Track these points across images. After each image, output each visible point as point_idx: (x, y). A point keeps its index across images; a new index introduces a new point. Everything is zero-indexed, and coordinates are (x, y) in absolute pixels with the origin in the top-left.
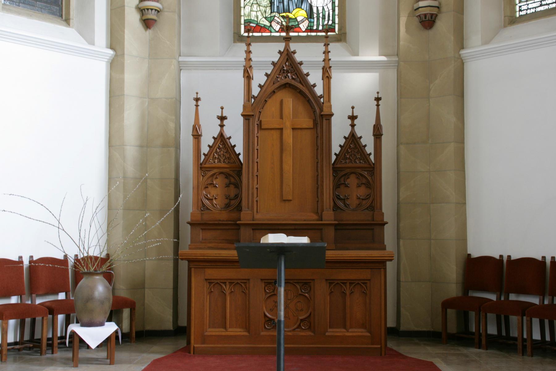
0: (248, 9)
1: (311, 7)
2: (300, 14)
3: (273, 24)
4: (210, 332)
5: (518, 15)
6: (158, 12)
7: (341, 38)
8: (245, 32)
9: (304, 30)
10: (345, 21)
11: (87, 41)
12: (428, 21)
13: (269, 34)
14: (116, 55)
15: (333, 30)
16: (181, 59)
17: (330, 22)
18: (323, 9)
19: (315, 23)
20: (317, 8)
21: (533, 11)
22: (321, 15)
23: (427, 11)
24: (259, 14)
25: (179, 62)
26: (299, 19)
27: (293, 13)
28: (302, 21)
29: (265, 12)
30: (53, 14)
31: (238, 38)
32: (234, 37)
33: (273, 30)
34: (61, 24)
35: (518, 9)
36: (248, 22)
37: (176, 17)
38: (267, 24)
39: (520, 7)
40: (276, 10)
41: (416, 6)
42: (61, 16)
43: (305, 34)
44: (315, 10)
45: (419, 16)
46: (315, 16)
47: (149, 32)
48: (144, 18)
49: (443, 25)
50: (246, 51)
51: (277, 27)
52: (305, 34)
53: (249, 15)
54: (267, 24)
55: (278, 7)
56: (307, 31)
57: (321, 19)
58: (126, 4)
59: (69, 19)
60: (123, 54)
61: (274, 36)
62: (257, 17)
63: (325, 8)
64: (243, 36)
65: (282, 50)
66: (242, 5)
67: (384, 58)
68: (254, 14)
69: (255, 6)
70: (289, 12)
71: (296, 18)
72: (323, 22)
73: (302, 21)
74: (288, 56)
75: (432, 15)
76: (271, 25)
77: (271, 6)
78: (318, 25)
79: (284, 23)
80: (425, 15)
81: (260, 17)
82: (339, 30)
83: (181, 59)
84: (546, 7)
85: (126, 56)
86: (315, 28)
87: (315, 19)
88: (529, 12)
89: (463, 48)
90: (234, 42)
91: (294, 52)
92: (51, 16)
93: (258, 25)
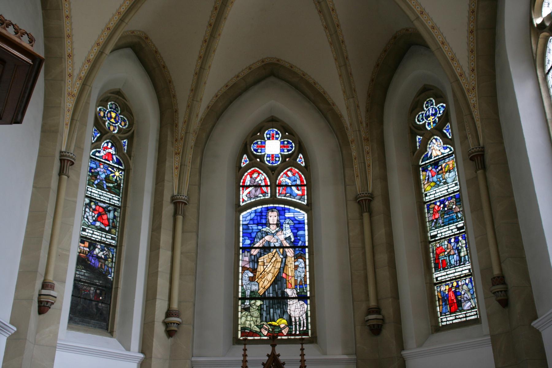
0: (243, 319)
1: (290, 317)
2: (282, 322)
3: (263, 330)
4: (470, 316)
5: (440, 325)
6: (179, 324)
7: (313, 340)
8: (241, 336)
9: (285, 334)
10: (315, 327)
11: (124, 348)
12: (376, 330)
13: (259, 338)
14: (145, 358)
15: (307, 335)
16: (193, 359)
17: (305, 328)
18: (299, 318)
19: (294, 329)
20: (295, 317)
21: (451, 322)
22: (298, 323)
23: (375, 322)
24: (252, 323)
25: (192, 361)
26: (282, 326)
27: (277, 321)
28: (284, 328)
29: (256, 321)
30: (101, 328)
31: (237, 341)
32: (233, 340)
33: (262, 335)
34: (106, 336)
35: (440, 320)
36: (243, 329)
37: (191, 328)
38: (258, 330)
39: (441, 319)
40: (264, 320)
41: (366, 318)
42: (107, 329)
43: (286, 337)
44: (293, 320)
45: (369, 326)
46: (294, 323)
47: (171, 339)
48: (168, 329)
49: (388, 332)
50: (243, 355)
51: (266, 333)
52: (286, 337)
53: (245, 323)
54: (258, 330)
55: (266, 317)
56: (287, 335)
57: (298, 326)
58: (156, 320)
59: (113, 332)
60: (151, 358)
61: (263, 339)
62: (250, 325)
63: (301, 318)
64: (239, 339)
65: (270, 354)
66: (240, 316)
67: (346, 357)
68: (248, 323)
69: (249, 317)
70: (274, 321)
71: (279, 326)
72: (300, 328)
73: (284, 328)
74: (273, 357)
75: (378, 325)
76: (261, 331)
77: (261, 317)
78: (296, 330)
79: (270, 329)
80: (374, 325)
81: (253, 325)
82: (311, 334)
83: (193, 359)
84: (459, 320)
85: (153, 359)
86: (294, 333)
87: (294, 326)
88: (448, 323)
89: (403, 349)
90: (233, 345)
91: (279, 355)
92: (100, 330)
93: (251, 331)
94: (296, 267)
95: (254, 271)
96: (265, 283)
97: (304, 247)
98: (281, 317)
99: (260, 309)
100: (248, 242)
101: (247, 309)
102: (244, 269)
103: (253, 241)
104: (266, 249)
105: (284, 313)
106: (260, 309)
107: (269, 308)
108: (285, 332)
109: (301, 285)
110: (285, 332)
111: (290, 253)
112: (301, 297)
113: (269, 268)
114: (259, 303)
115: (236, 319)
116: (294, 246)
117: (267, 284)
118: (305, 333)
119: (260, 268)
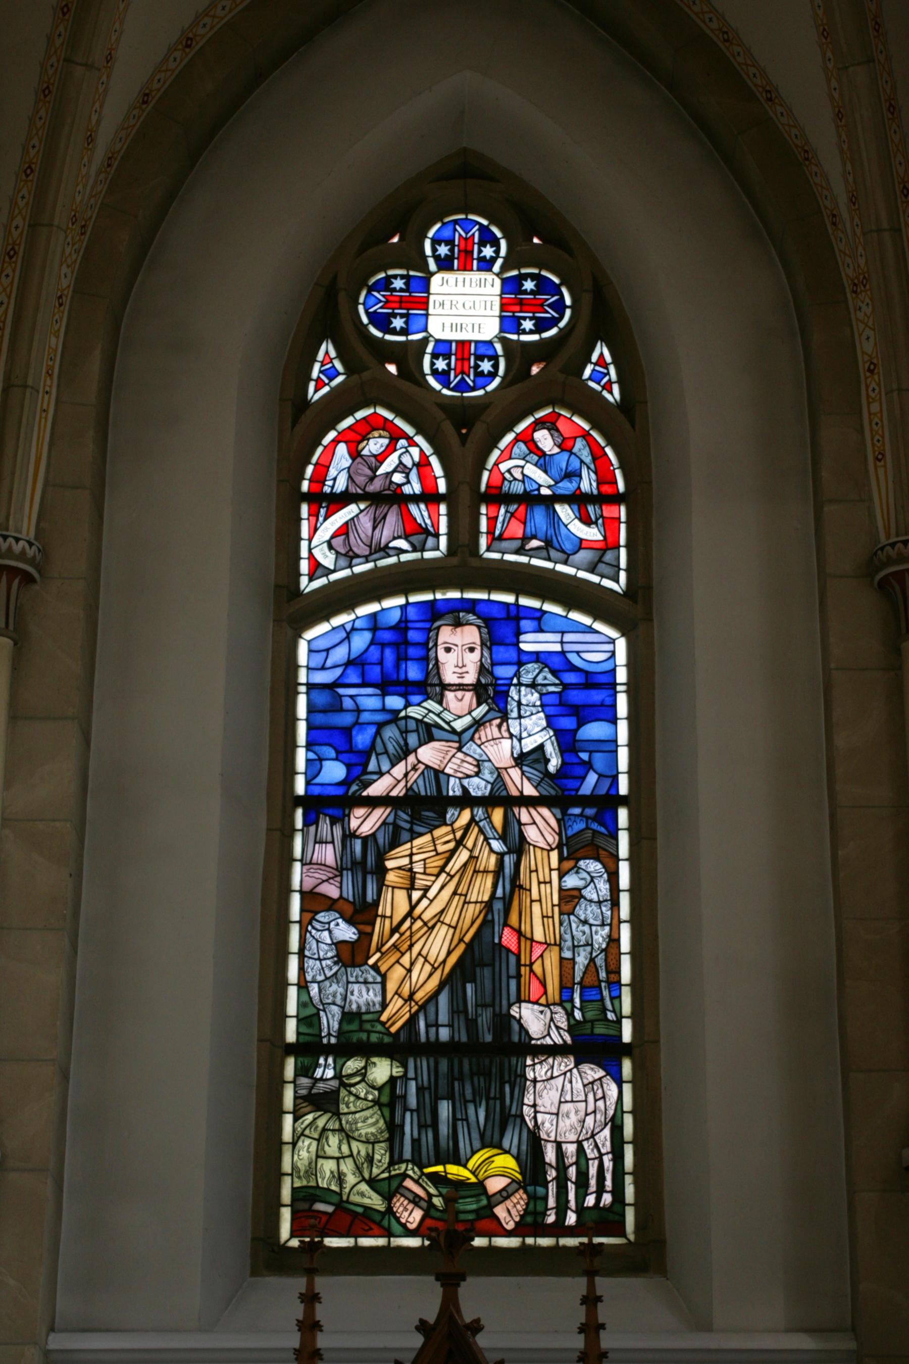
31: (269, 1257)
94: (570, 899)
95: (362, 913)
96: (419, 968)
97: (609, 802)
98: (491, 1140)
99: (390, 1099)
100: (334, 771)
101: (323, 1101)
102: (314, 902)
103: (359, 767)
104: (425, 806)
105: (505, 1120)
106: (390, 1099)
107: (430, 1095)
108: (507, 1214)
109: (596, 984)
110: (507, 1214)
111: (540, 827)
112: (591, 1046)
113: (434, 901)
114: (382, 1070)
115: (270, 1145)
116: (559, 794)
117: (423, 979)
118: (607, 1220)
119: (395, 903)
